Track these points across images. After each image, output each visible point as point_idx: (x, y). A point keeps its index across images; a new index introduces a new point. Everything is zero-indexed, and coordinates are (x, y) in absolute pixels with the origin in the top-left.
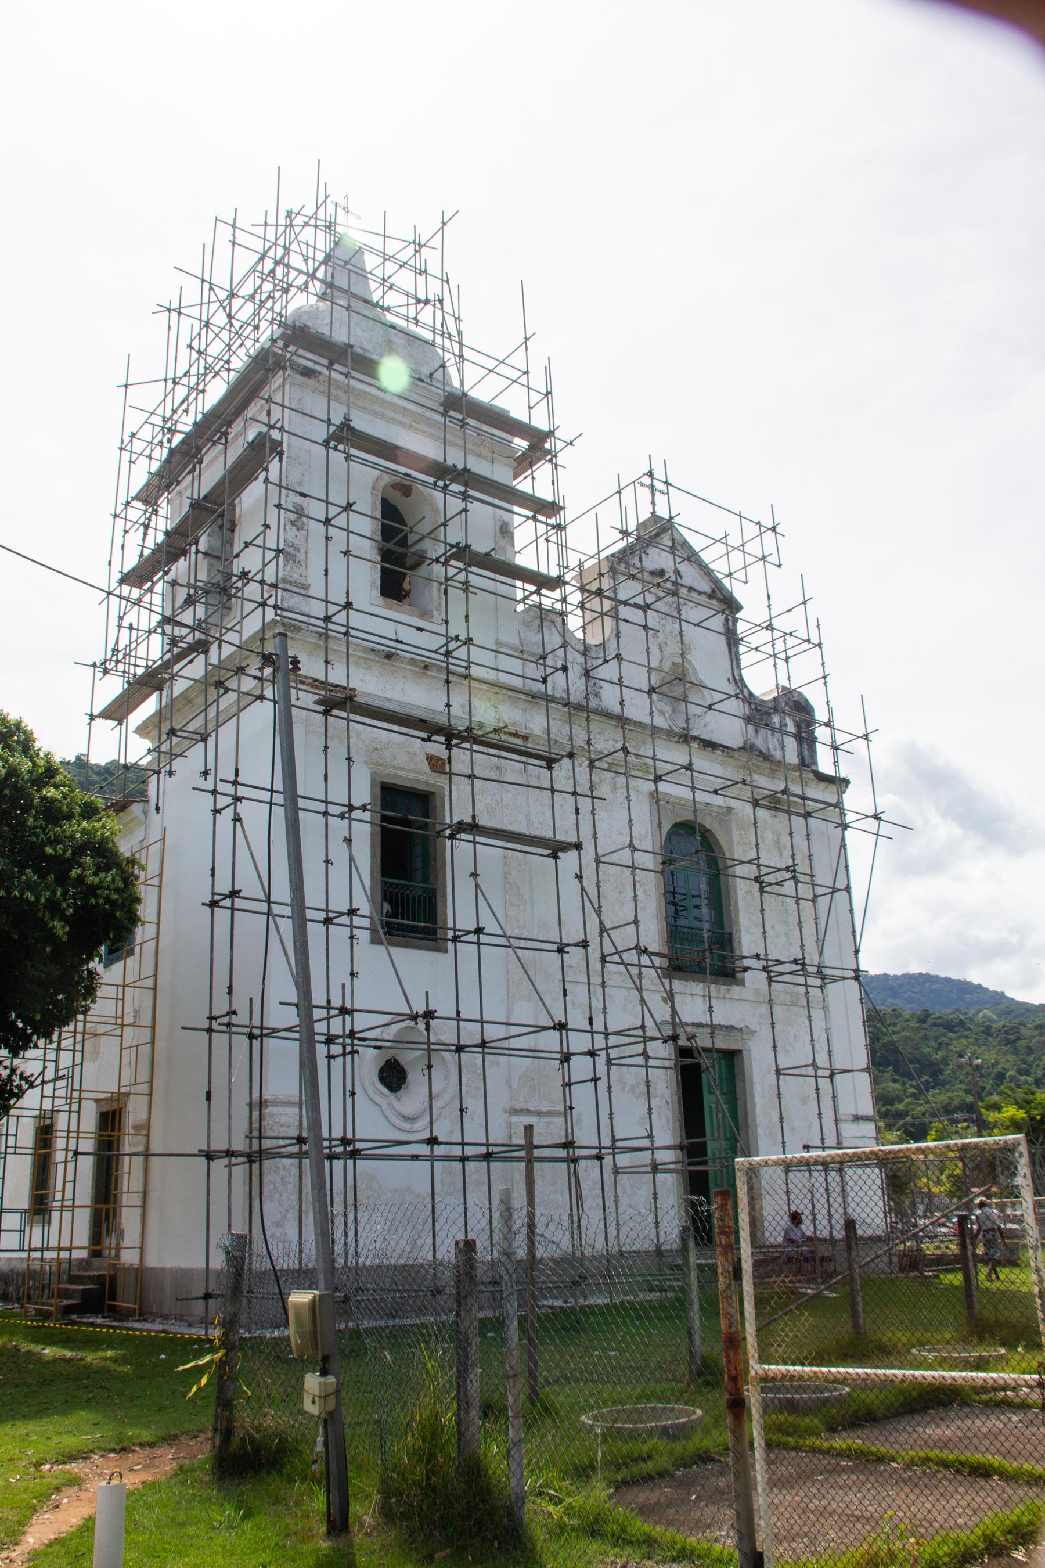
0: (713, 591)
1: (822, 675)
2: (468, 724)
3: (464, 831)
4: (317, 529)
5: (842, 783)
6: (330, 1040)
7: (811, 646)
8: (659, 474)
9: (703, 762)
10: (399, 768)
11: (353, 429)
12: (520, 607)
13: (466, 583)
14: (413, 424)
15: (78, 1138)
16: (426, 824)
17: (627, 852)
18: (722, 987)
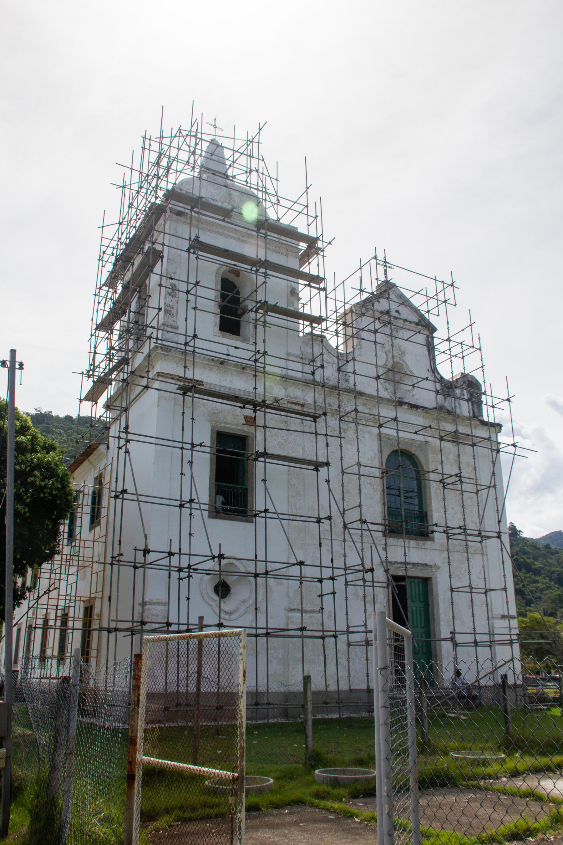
0: (420, 321)
1: (481, 365)
2: (263, 398)
3: (261, 457)
4: (183, 296)
5: (498, 427)
6: (180, 570)
7: (474, 349)
8: (380, 257)
9: (404, 414)
10: (227, 423)
11: (201, 242)
12: (301, 335)
13: (265, 322)
14: (241, 238)
15: (74, 621)
16: (244, 453)
17: (356, 467)
18: (420, 542)
